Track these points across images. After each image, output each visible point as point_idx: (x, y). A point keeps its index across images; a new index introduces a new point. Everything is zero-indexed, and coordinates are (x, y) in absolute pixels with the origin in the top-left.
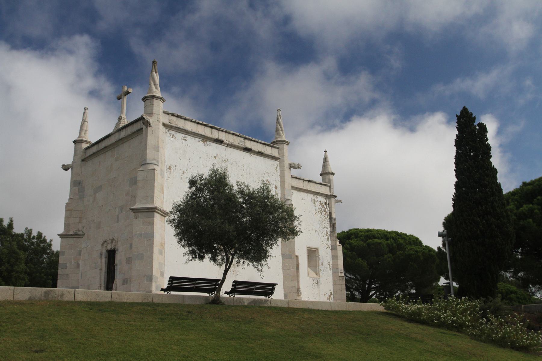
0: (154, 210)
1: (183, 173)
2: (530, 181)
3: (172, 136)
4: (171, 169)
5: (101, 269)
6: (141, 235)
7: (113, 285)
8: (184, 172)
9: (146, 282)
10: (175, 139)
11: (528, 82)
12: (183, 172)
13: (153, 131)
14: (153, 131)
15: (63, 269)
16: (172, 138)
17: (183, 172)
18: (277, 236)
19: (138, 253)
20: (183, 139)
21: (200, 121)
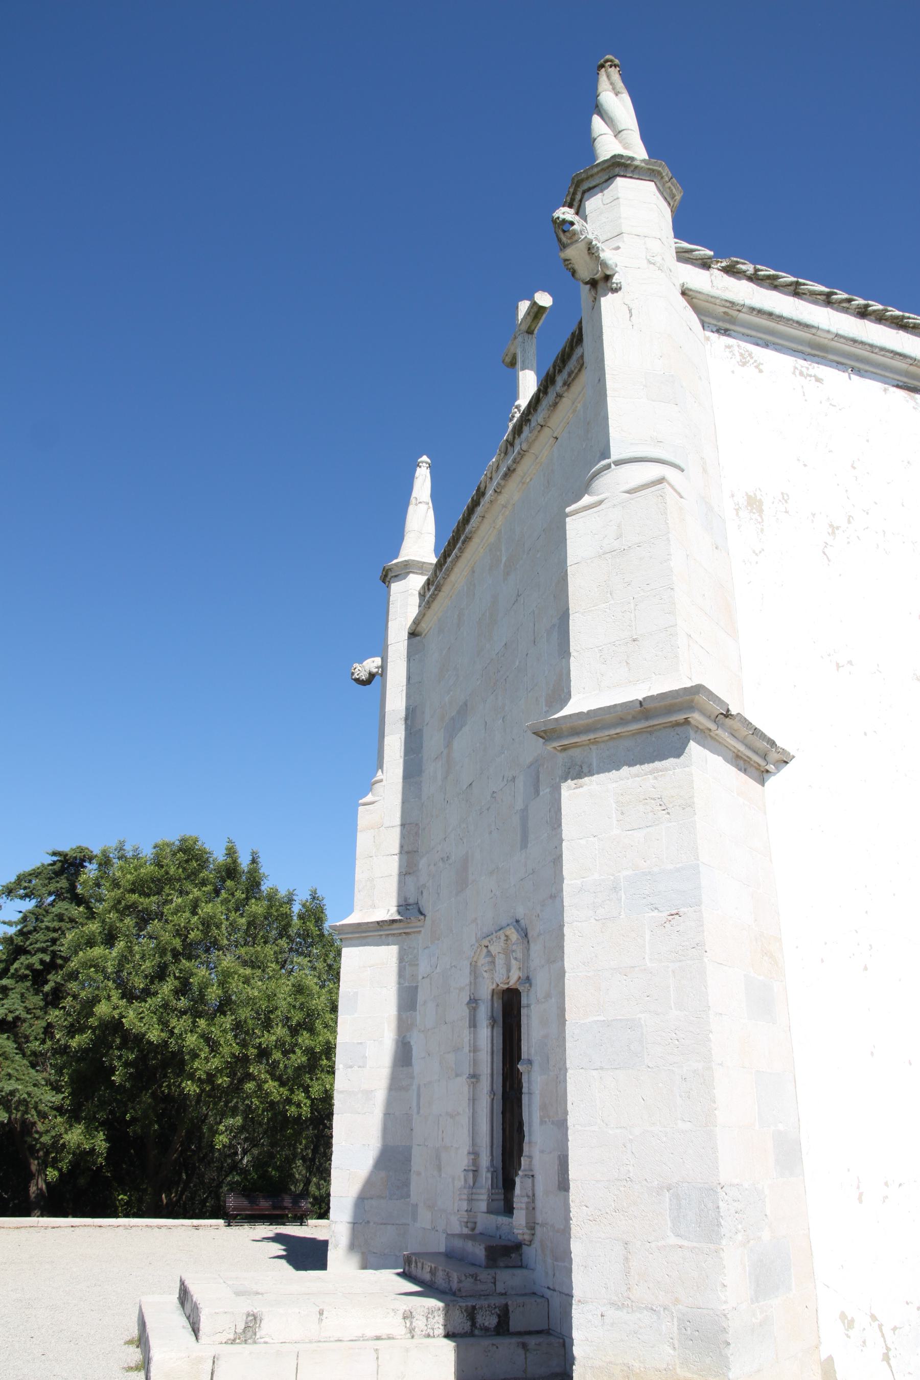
0: (680, 717)
1: (833, 533)
2: (395, 1037)
3: (741, 355)
4: (761, 511)
5: (474, 1077)
6: (615, 889)
7: (522, 1159)
8: (833, 529)
9: (673, 1240)
10: (761, 371)
11: (204, 1210)
12: (831, 526)
13: (630, 311)
14: (630, 311)
15: (351, 1067)
16: (744, 364)
17: (831, 526)
18: (77, 1052)
19: (601, 1018)
20: (801, 374)
21: (871, 302)
